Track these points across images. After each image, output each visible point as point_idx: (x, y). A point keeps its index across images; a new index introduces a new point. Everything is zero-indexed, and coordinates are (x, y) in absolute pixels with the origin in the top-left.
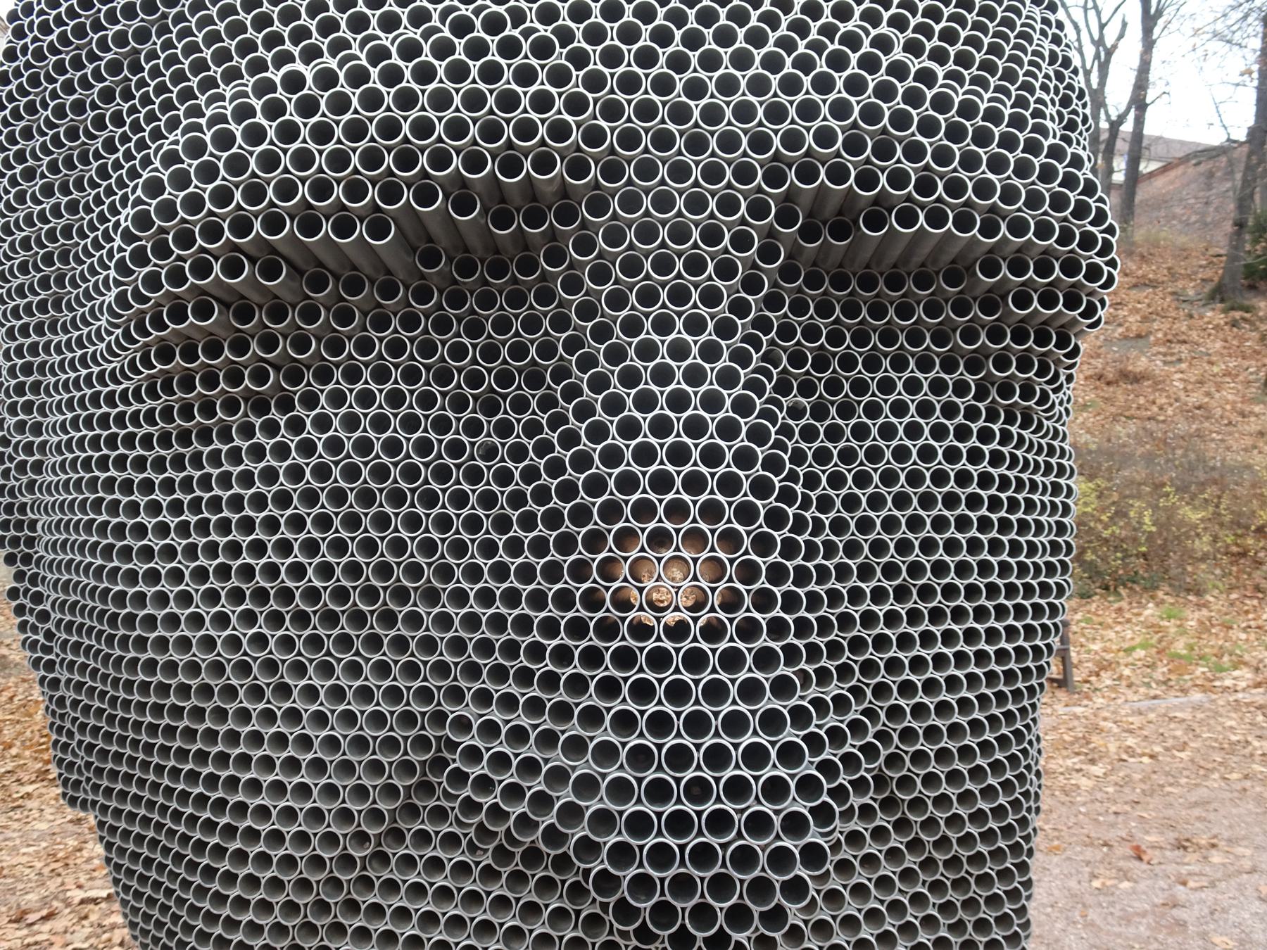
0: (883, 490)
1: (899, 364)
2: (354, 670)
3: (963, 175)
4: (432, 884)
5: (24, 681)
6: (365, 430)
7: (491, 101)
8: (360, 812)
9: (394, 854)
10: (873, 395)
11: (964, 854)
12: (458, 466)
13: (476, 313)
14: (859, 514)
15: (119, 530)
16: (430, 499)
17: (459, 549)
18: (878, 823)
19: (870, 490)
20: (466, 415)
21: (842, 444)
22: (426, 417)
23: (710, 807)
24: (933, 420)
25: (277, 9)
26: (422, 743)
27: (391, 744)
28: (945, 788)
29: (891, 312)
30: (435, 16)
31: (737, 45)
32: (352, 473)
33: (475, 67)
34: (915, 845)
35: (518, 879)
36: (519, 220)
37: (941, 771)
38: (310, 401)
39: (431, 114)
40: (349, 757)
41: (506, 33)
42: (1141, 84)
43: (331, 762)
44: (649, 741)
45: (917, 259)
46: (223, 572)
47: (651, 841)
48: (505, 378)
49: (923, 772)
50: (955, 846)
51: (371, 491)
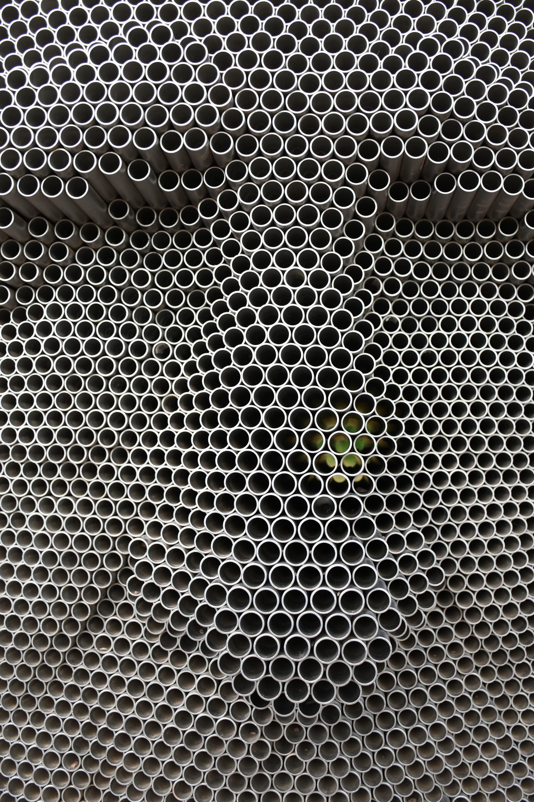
0: (454, 384)
1: (469, 291)
3: (512, 148)
4: (120, 658)
6: (74, 334)
7: (157, 93)
8: (70, 606)
9: (95, 636)
10: (449, 313)
11: (507, 649)
12: (140, 362)
13: (154, 250)
14: (435, 401)
16: (120, 385)
17: (140, 421)
18: (443, 625)
19: (444, 384)
20: (147, 325)
21: (424, 350)
22: (118, 325)
23: (302, 612)
24: (493, 333)
25: (10, 25)
26: (114, 559)
27: (91, 559)
28: (493, 601)
29: (463, 251)
30: (121, 30)
31: (342, 50)
32: (64, 365)
33: (145, 67)
34: (471, 642)
35: (179, 657)
36: (181, 182)
37: (491, 589)
38: (37, 313)
39: (113, 103)
40: (63, 567)
41: (170, 42)
43: (51, 570)
44: (261, 564)
45: (480, 213)
47: (259, 635)
48: (175, 298)
49: (477, 590)
50: (501, 643)
51: (78, 379)
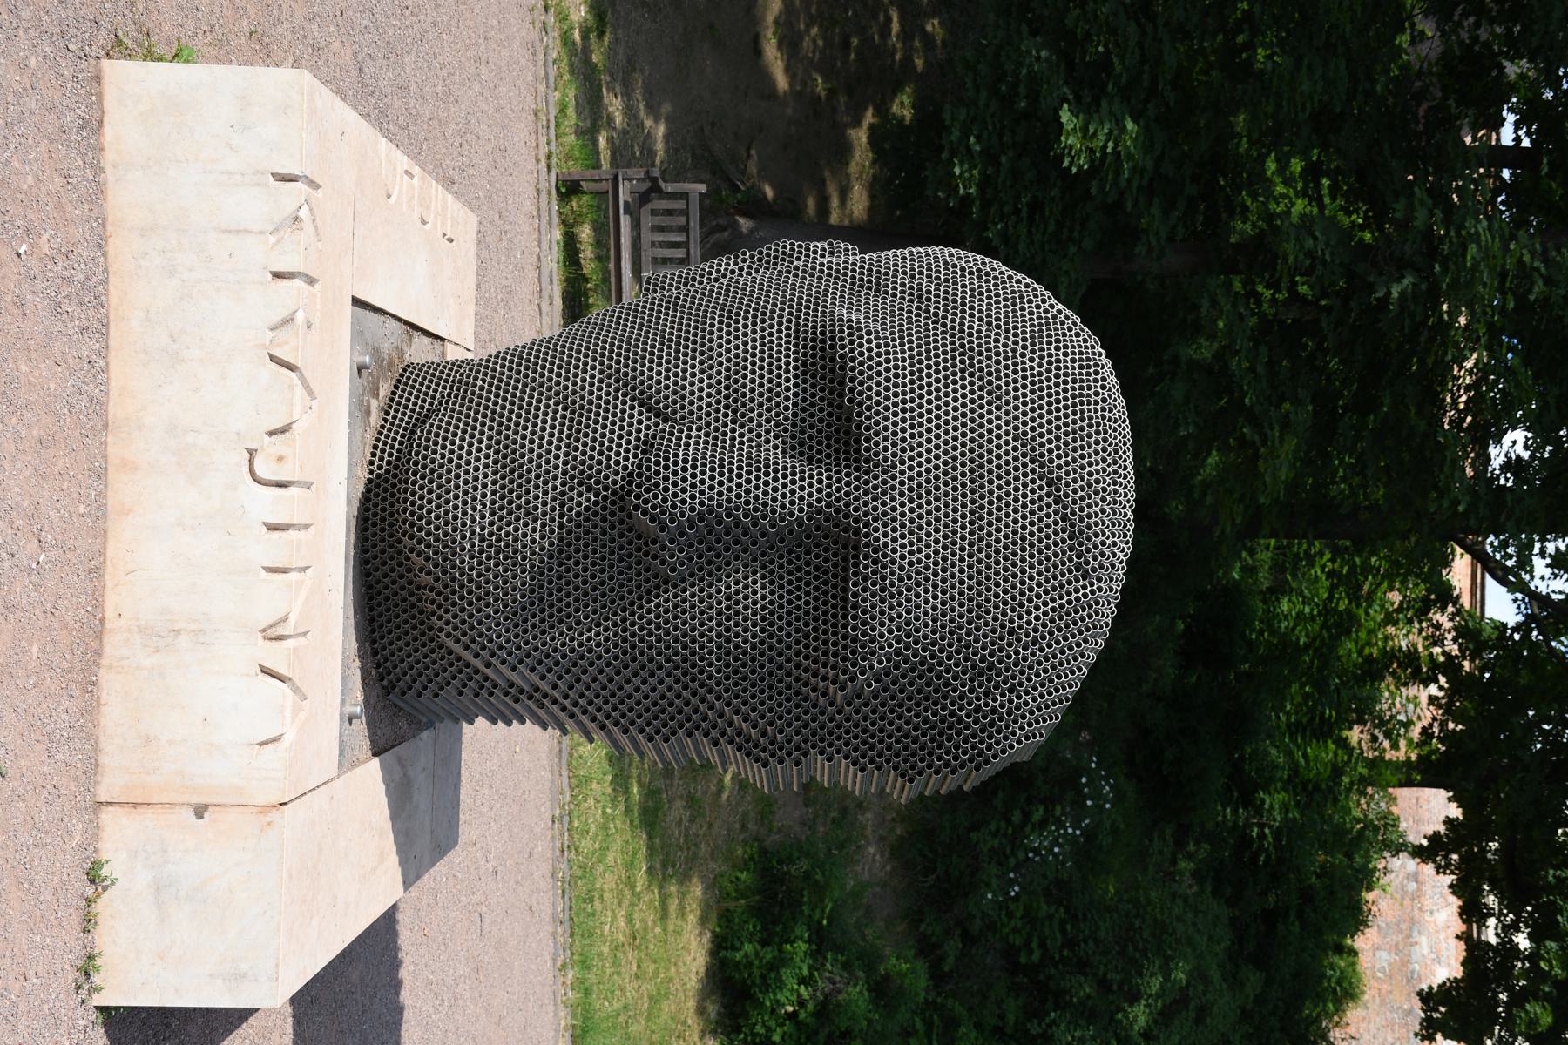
42: (560, 759)
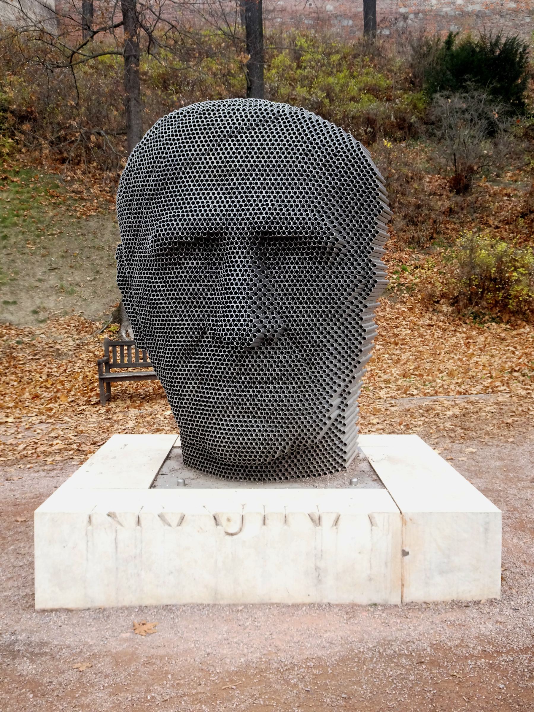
2: (192, 312)
5: (70, 362)
15: (151, 287)
38: (183, 264)
46: (170, 294)
